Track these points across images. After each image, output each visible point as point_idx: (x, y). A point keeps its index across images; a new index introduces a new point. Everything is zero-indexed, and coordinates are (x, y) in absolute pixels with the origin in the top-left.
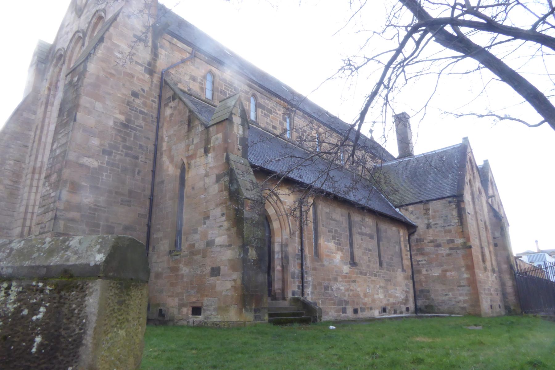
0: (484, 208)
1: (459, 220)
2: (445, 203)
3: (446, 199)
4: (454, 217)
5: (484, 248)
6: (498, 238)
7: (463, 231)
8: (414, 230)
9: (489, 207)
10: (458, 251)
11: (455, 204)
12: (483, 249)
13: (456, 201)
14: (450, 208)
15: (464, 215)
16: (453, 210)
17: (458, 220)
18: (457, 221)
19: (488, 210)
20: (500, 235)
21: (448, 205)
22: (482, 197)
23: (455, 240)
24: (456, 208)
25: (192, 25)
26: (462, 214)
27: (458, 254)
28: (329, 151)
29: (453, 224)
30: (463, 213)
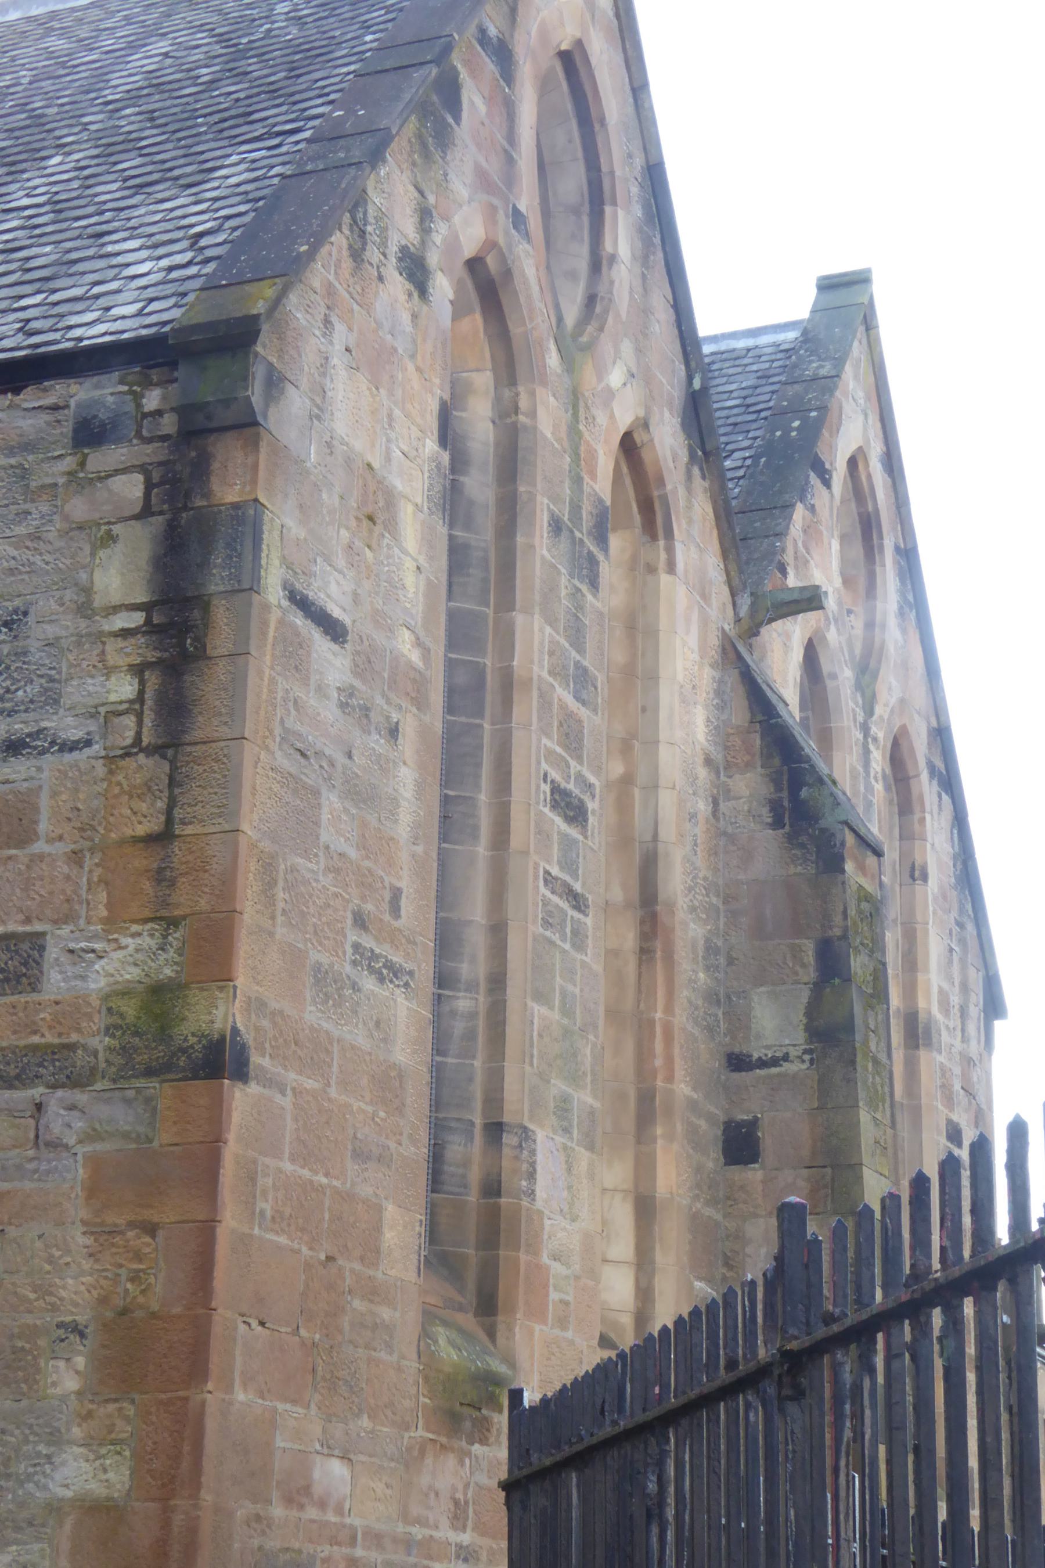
0: (667, 696)
1: (153, 679)
2: (27, 447)
3: (58, 390)
4: (100, 637)
5: (526, 1134)
6: (775, 1062)
7: (164, 837)
8: (945, 1355)
9: (739, 714)
10: (56, 1100)
11: (150, 453)
12: (509, 1139)
13: (169, 424)
14: (78, 508)
15: (221, 614)
16: (111, 538)
17: (139, 670)
18: (124, 688)
19: (720, 733)
20: (800, 1037)
21: (69, 463)
22: (671, 568)
23: (53, 952)
24: (146, 512)
25: (883, 464)
26: (204, 604)
27: (56, 1145)
28: (978, 970)
29: (76, 734)
30: (216, 582)
